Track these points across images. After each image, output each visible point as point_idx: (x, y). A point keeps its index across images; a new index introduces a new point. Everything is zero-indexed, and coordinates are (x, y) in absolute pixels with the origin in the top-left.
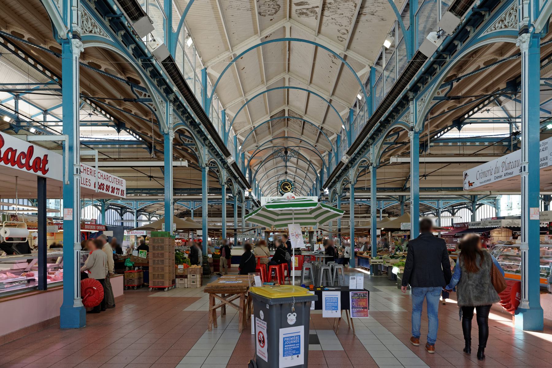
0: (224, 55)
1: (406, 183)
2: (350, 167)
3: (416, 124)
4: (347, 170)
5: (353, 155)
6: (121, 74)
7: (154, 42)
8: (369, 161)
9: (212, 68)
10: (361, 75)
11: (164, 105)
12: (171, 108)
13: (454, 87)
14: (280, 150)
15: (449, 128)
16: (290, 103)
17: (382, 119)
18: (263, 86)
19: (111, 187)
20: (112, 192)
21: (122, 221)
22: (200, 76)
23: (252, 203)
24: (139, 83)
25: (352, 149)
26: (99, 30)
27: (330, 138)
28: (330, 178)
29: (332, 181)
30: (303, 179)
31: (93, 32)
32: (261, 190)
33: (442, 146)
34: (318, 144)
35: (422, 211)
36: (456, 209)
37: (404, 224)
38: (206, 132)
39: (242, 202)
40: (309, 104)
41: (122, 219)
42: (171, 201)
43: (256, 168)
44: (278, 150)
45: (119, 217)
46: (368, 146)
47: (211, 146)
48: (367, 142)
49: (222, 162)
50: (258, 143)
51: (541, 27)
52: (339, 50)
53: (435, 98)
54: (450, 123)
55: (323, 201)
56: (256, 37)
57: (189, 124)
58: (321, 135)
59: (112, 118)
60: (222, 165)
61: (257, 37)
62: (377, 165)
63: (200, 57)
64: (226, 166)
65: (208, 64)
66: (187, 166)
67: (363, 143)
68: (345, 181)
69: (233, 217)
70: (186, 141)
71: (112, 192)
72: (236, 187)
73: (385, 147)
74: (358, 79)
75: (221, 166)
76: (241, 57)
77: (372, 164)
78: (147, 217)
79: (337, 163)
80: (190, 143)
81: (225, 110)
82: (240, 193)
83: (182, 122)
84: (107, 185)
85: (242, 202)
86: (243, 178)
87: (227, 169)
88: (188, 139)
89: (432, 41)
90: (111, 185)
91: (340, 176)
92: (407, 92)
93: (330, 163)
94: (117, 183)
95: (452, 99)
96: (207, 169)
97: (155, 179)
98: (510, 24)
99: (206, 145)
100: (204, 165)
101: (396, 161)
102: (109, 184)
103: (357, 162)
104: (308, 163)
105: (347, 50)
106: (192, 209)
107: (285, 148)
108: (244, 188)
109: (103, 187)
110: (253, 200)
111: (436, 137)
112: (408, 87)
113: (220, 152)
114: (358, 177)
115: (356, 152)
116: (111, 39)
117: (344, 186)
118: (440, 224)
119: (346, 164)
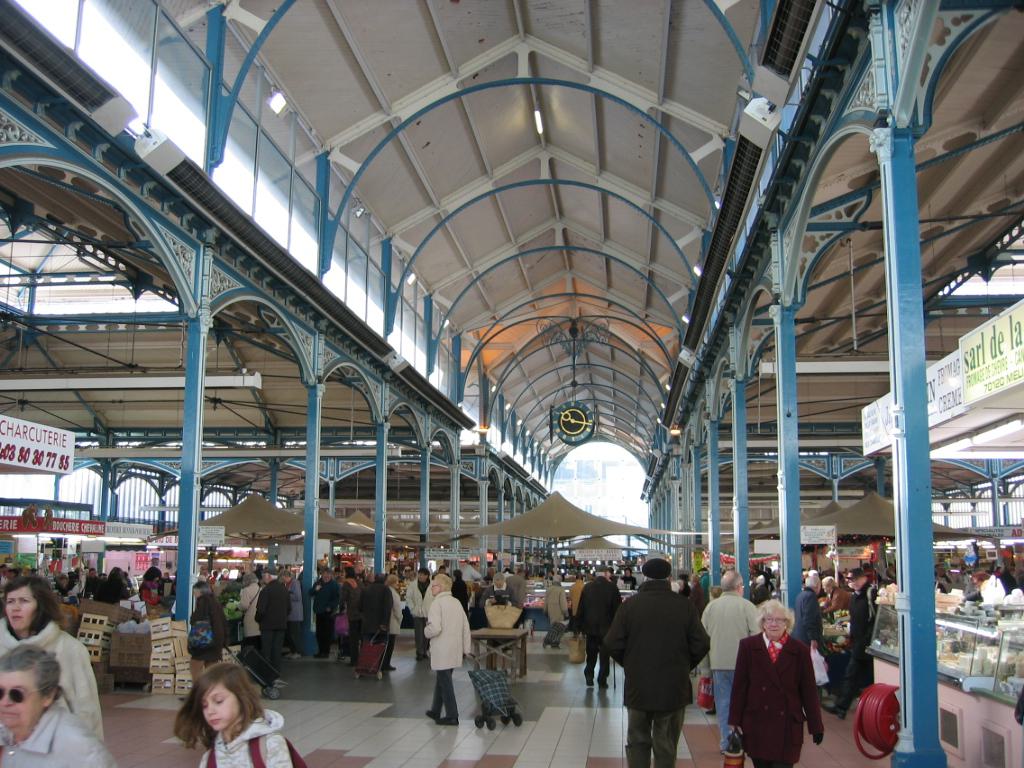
0: (375, 120)
2: (708, 377)
7: (148, 139)
9: (344, 150)
10: (701, 157)
14: (558, 325)
15: (966, 274)
19: (32, 452)
20: (34, 463)
21: (162, 509)
26: (18, 133)
27: (672, 300)
30: (635, 398)
32: (545, 455)
33: (963, 316)
34: (651, 311)
35: (941, 486)
36: (1011, 483)
37: (809, 528)
39: (451, 463)
41: (163, 503)
42: (195, 476)
43: (499, 372)
45: (155, 499)
49: (376, 367)
50: (495, 311)
51: (907, 113)
52: (644, 99)
54: (962, 264)
56: (447, 78)
59: (121, 265)
61: (449, 79)
62: (746, 376)
69: (417, 497)
70: (273, 323)
71: (34, 463)
72: (426, 425)
76: (417, 120)
78: (228, 497)
83: (242, 286)
84: (22, 449)
85: (451, 463)
89: (758, 117)
90: (33, 447)
94: (52, 441)
95: (871, 228)
97: (225, 404)
102: (27, 444)
105: (663, 101)
106: (332, 479)
107: (571, 320)
109: (13, 453)
111: (941, 293)
116: (48, 144)
118: (629, 545)
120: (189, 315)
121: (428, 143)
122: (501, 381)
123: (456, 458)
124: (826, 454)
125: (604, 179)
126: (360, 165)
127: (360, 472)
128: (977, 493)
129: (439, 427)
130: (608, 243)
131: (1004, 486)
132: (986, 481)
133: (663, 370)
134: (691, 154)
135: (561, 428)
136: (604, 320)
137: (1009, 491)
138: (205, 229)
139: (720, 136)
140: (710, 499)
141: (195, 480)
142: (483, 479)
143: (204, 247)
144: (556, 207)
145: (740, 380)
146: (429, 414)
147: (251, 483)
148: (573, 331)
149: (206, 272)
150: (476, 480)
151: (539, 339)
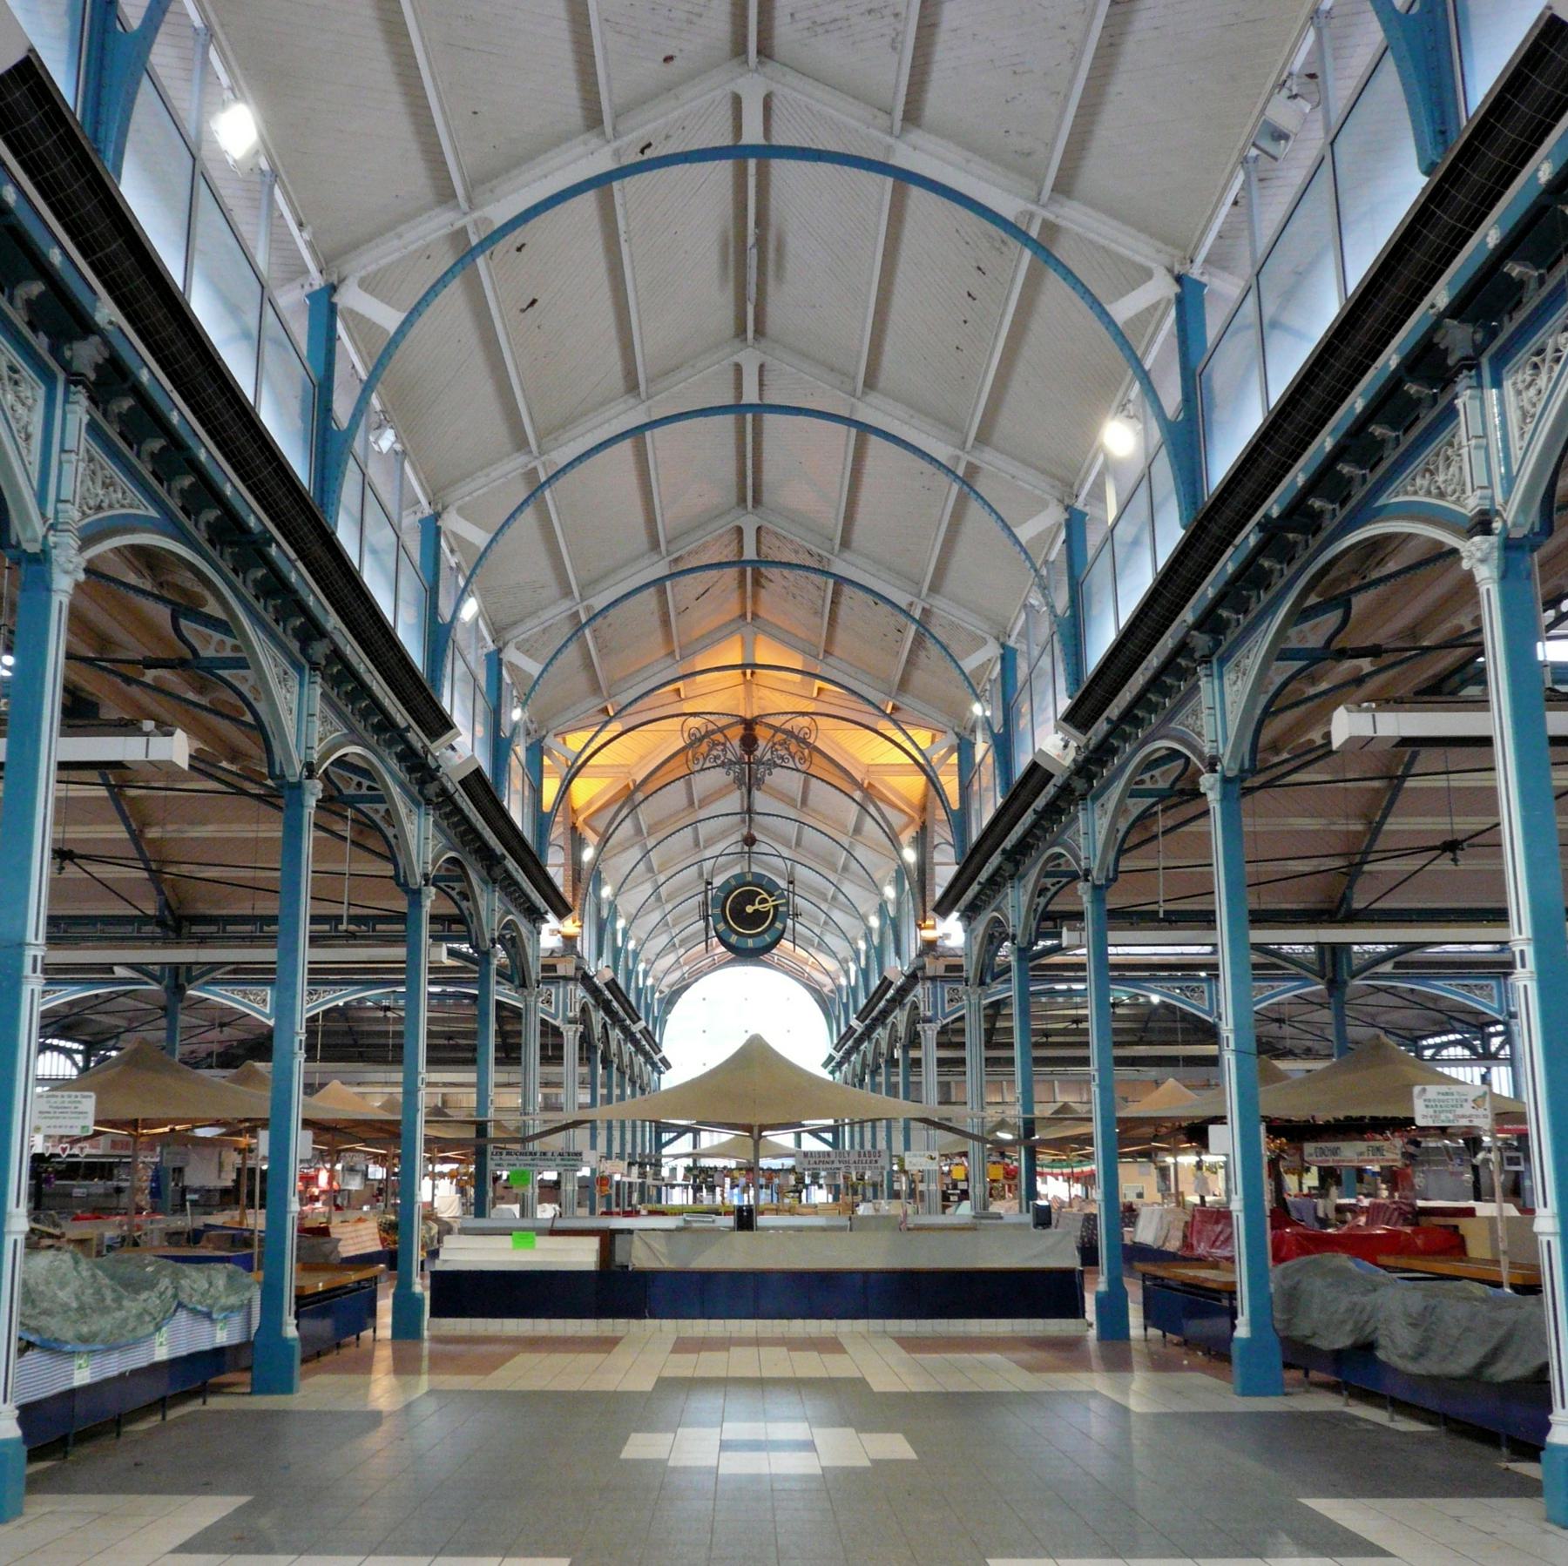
0: (508, 467)
1: (1350, 887)
3: (1508, 492)
4: (1061, 812)
5: (1101, 727)
6: (140, 574)
8: (1078, 861)
11: (25, 391)
12: (78, 412)
13: (1353, 612)
14: (721, 730)
16: (766, 497)
17: (1273, 506)
18: (656, 558)
22: (414, 544)
23: (580, 992)
24: (204, 603)
25: (1088, 705)
26: (120, 495)
28: (970, 862)
29: (983, 876)
31: (105, 505)
32: (636, 954)
34: (906, 700)
36: (1429, 1047)
38: (314, 598)
39: (523, 985)
40: (865, 495)
43: (601, 825)
44: (708, 734)
46: (1445, 379)
47: (341, 678)
48: (1182, 648)
53: (1285, 655)
55: (933, 979)
57: (201, 536)
58: (922, 654)
60: (415, 789)
63: (300, 225)
64: (432, 789)
65: (508, 636)
66: (186, 767)
67: (1154, 660)
68: (1049, 875)
72: (491, 908)
73: (1137, 806)
74: (1119, 335)
75: (402, 785)
77: (1212, 765)
78: (75, 1064)
79: (963, 852)
80: (364, 791)
81: (332, 289)
82: (514, 945)
83: (153, 513)
85: (523, 985)
86: (534, 865)
87: (438, 807)
88: (356, 779)
91: (1023, 848)
92: (1436, 326)
93: (965, 788)
96: (314, 792)
98: (1450, 489)
99: (315, 667)
100: (296, 771)
101: (1368, 732)
103: (1122, 769)
104: (858, 795)
108: (536, 916)
110: (586, 980)
112: (1440, 296)
113: (401, 717)
114: (1121, 852)
115: (1114, 710)
117: (1042, 901)
119: (1058, 780)
120: (25, 546)
121: (534, 302)
122: (605, 840)
123: (534, 977)
124: (201, 1132)
125: (870, 405)
126: (403, 316)
127: (326, 1012)
128: (1428, 1053)
129: (509, 912)
130: (847, 555)
131: (1482, 1040)
132: (1497, 1022)
133: (905, 819)
134: (1108, 308)
135: (727, 922)
136: (804, 721)
137: (1493, 1049)
138: (71, 339)
139: (1170, 270)
140: (1018, 1062)
141: (28, 962)
142: (572, 1021)
143: (68, 382)
144: (750, 481)
145: (1230, 774)
146: (495, 881)
147: (117, 1036)
148: (749, 742)
149: (71, 443)
150: (556, 1023)
151: (681, 759)
